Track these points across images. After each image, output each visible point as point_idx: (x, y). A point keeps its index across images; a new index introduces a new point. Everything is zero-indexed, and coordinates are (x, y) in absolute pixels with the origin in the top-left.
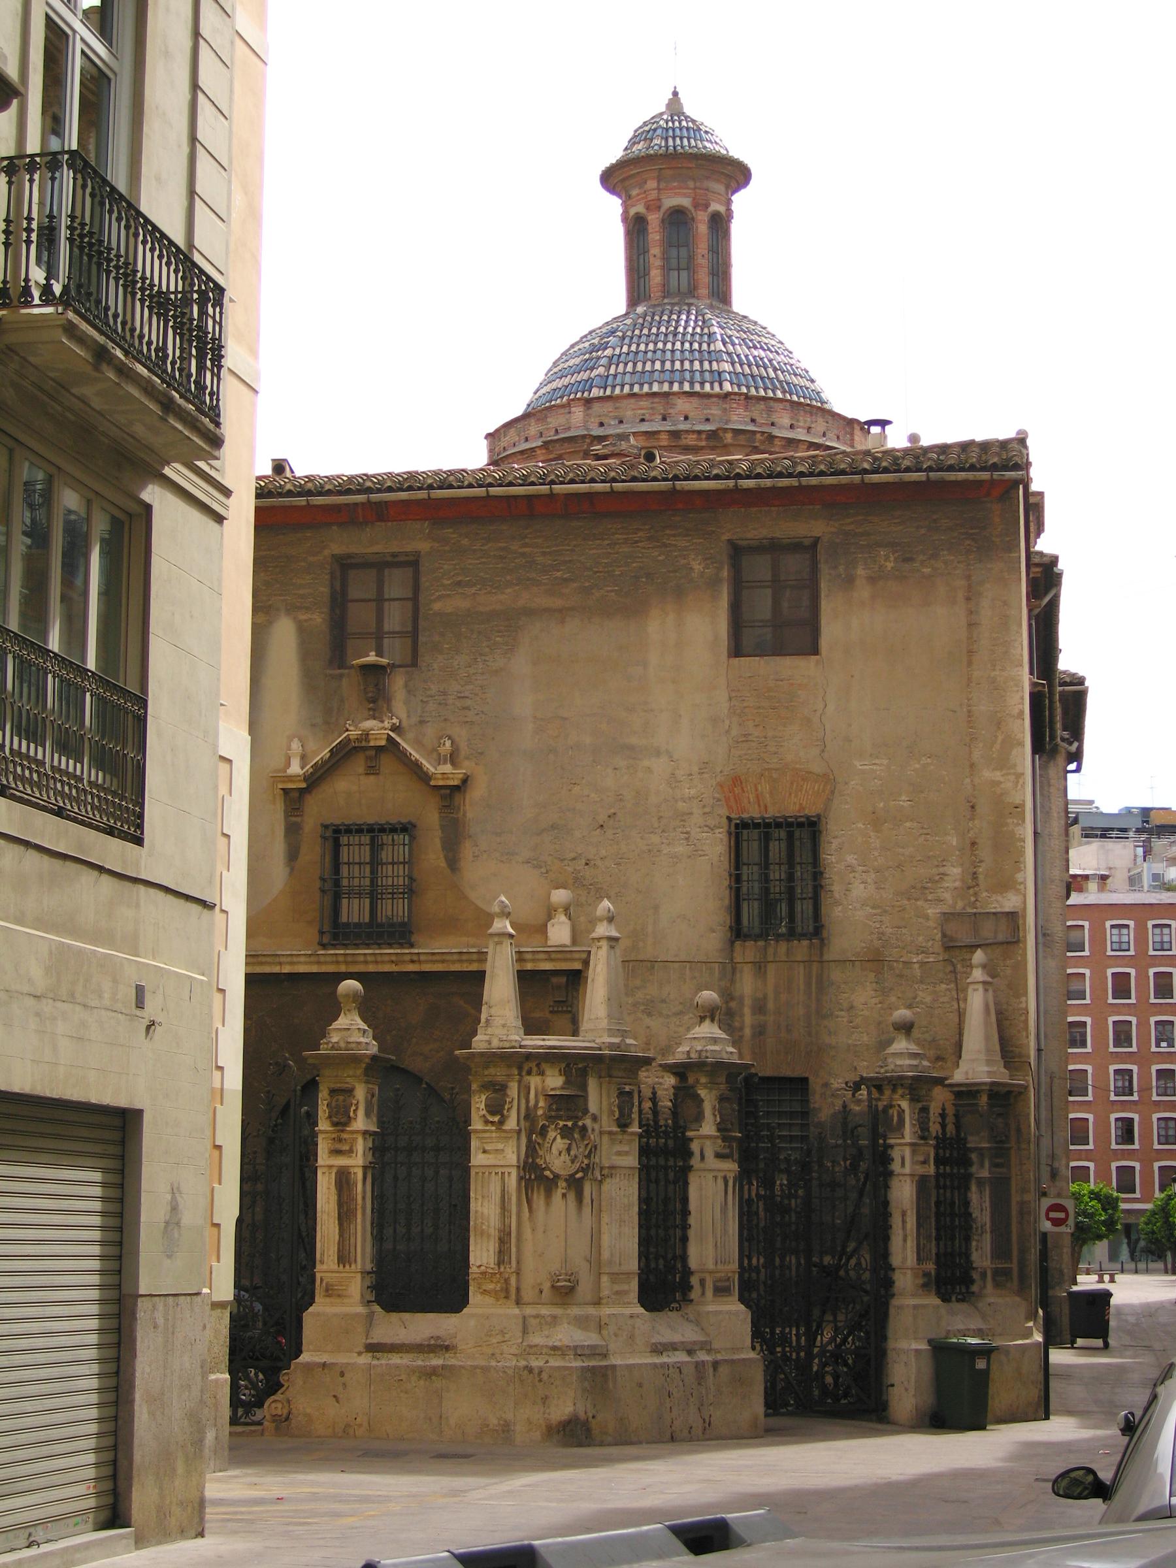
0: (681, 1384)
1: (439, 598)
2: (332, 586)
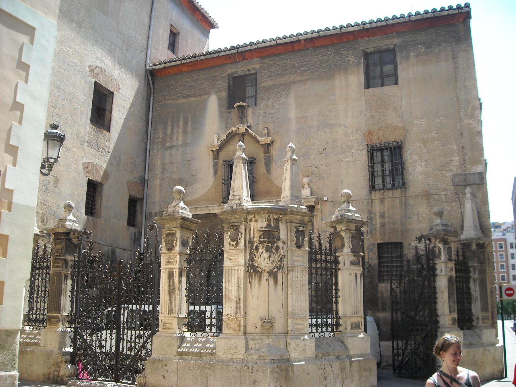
0: (332, 373)
1: (263, 82)
2: (229, 83)
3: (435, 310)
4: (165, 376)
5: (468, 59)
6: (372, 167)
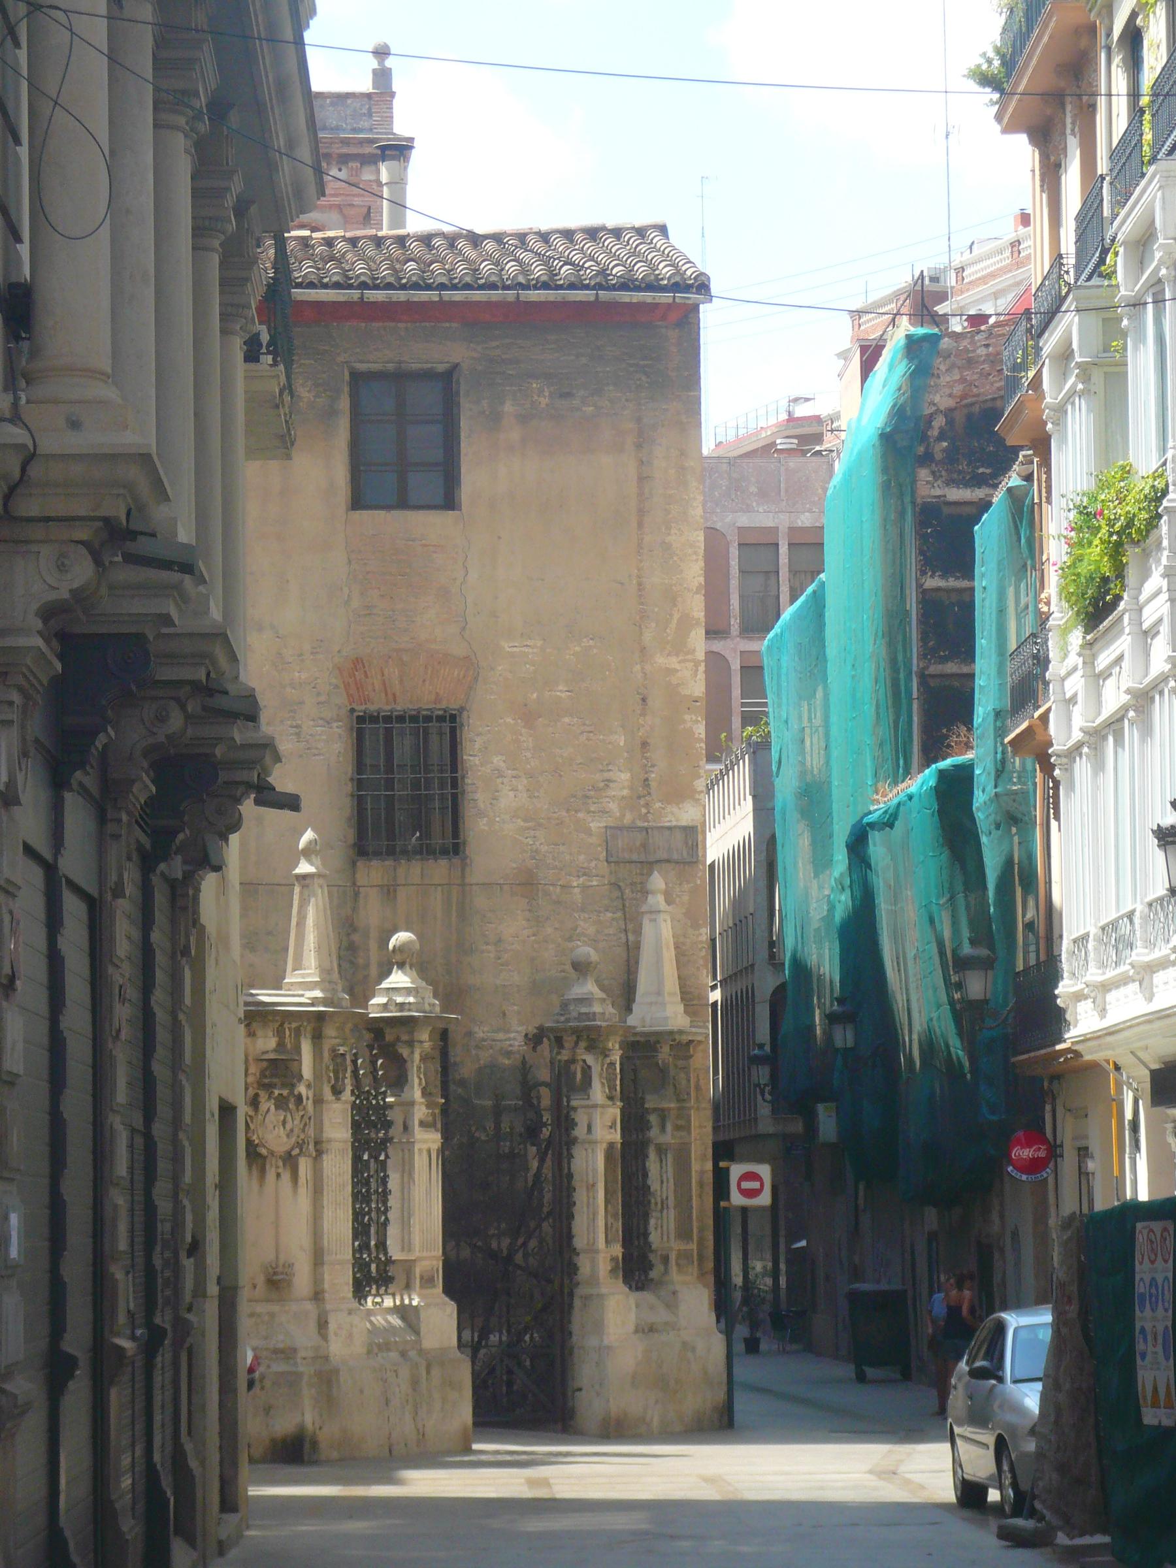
3: (570, 1236)
5: (683, 453)
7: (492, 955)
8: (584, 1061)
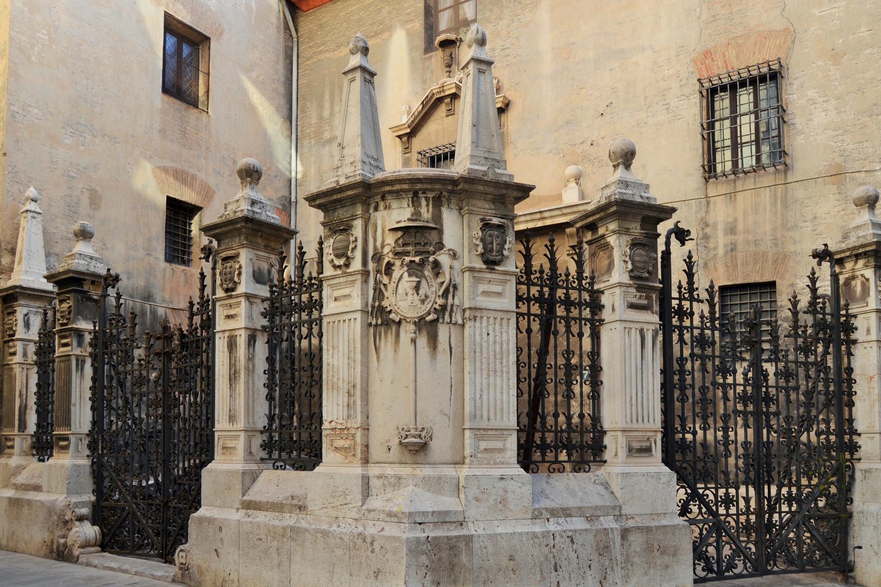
0: (573, 555)
4: (219, 551)
6: (711, 126)
7: (809, 229)
8: (862, 275)
